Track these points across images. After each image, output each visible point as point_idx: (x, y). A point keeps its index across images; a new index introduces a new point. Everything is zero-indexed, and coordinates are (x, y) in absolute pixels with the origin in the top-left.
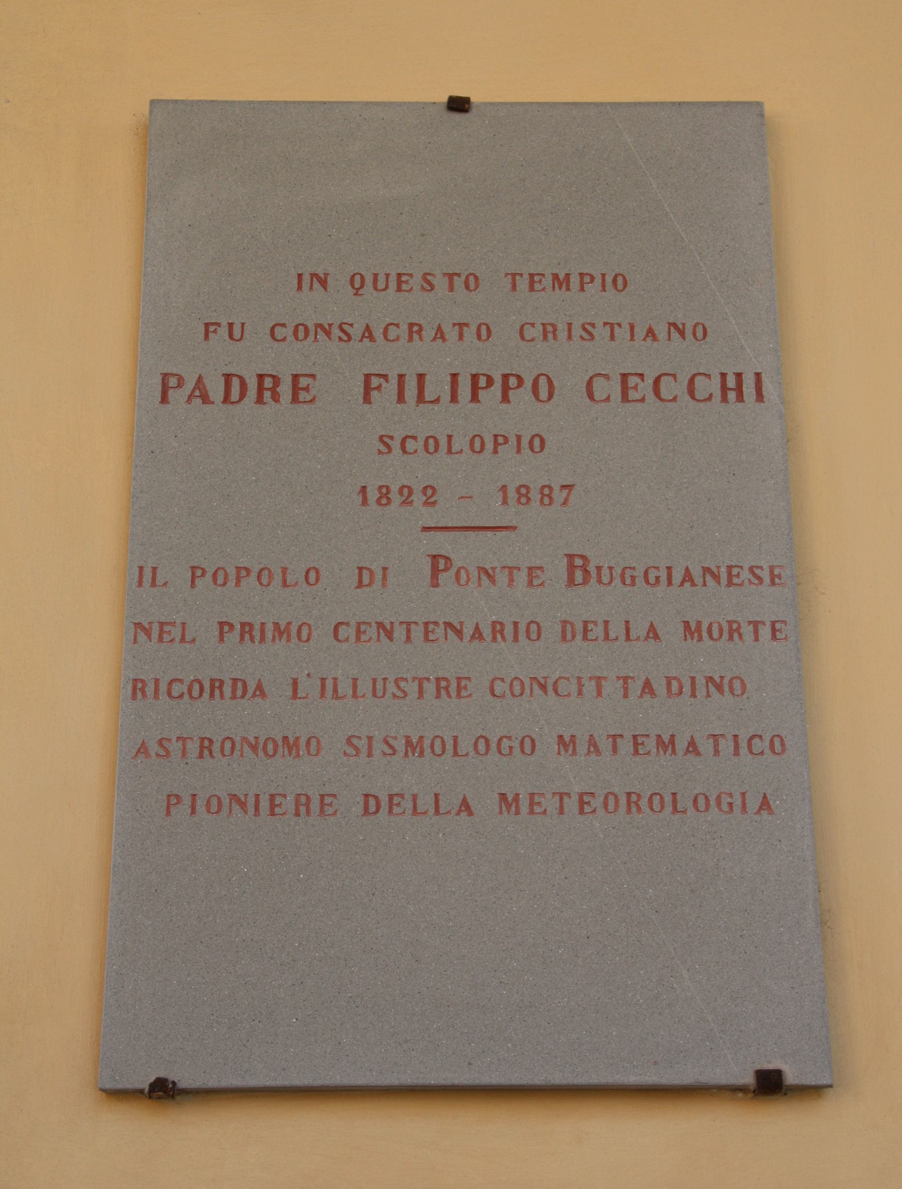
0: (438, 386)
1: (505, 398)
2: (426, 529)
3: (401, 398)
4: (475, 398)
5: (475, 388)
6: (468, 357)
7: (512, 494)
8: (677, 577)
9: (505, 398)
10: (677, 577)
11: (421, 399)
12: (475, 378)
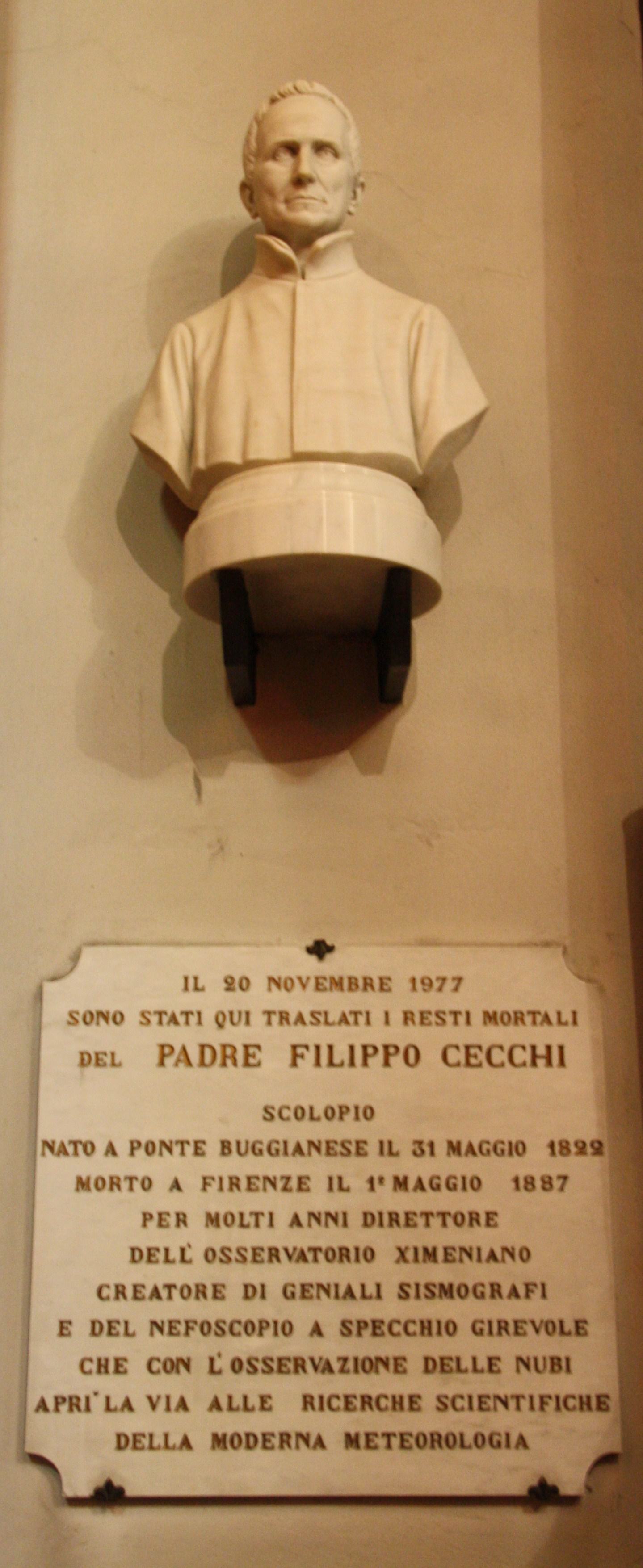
0: (341, 1054)
1: (387, 1063)
2: (387, 1014)
3: (318, 1063)
4: (365, 1063)
5: (366, 1056)
6: (360, 1035)
7: (522, 1183)
8: (291, 1148)
9: (387, 1063)
10: (291, 1148)
11: (331, 1063)
12: (365, 1048)
